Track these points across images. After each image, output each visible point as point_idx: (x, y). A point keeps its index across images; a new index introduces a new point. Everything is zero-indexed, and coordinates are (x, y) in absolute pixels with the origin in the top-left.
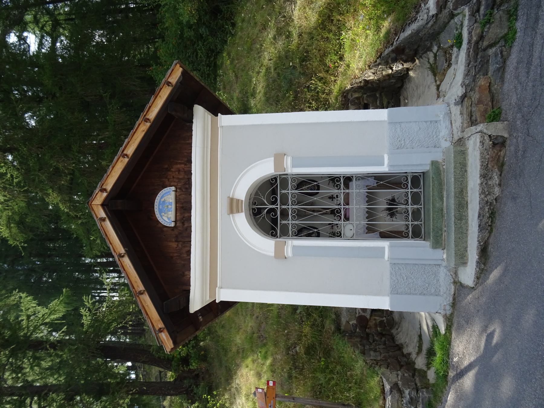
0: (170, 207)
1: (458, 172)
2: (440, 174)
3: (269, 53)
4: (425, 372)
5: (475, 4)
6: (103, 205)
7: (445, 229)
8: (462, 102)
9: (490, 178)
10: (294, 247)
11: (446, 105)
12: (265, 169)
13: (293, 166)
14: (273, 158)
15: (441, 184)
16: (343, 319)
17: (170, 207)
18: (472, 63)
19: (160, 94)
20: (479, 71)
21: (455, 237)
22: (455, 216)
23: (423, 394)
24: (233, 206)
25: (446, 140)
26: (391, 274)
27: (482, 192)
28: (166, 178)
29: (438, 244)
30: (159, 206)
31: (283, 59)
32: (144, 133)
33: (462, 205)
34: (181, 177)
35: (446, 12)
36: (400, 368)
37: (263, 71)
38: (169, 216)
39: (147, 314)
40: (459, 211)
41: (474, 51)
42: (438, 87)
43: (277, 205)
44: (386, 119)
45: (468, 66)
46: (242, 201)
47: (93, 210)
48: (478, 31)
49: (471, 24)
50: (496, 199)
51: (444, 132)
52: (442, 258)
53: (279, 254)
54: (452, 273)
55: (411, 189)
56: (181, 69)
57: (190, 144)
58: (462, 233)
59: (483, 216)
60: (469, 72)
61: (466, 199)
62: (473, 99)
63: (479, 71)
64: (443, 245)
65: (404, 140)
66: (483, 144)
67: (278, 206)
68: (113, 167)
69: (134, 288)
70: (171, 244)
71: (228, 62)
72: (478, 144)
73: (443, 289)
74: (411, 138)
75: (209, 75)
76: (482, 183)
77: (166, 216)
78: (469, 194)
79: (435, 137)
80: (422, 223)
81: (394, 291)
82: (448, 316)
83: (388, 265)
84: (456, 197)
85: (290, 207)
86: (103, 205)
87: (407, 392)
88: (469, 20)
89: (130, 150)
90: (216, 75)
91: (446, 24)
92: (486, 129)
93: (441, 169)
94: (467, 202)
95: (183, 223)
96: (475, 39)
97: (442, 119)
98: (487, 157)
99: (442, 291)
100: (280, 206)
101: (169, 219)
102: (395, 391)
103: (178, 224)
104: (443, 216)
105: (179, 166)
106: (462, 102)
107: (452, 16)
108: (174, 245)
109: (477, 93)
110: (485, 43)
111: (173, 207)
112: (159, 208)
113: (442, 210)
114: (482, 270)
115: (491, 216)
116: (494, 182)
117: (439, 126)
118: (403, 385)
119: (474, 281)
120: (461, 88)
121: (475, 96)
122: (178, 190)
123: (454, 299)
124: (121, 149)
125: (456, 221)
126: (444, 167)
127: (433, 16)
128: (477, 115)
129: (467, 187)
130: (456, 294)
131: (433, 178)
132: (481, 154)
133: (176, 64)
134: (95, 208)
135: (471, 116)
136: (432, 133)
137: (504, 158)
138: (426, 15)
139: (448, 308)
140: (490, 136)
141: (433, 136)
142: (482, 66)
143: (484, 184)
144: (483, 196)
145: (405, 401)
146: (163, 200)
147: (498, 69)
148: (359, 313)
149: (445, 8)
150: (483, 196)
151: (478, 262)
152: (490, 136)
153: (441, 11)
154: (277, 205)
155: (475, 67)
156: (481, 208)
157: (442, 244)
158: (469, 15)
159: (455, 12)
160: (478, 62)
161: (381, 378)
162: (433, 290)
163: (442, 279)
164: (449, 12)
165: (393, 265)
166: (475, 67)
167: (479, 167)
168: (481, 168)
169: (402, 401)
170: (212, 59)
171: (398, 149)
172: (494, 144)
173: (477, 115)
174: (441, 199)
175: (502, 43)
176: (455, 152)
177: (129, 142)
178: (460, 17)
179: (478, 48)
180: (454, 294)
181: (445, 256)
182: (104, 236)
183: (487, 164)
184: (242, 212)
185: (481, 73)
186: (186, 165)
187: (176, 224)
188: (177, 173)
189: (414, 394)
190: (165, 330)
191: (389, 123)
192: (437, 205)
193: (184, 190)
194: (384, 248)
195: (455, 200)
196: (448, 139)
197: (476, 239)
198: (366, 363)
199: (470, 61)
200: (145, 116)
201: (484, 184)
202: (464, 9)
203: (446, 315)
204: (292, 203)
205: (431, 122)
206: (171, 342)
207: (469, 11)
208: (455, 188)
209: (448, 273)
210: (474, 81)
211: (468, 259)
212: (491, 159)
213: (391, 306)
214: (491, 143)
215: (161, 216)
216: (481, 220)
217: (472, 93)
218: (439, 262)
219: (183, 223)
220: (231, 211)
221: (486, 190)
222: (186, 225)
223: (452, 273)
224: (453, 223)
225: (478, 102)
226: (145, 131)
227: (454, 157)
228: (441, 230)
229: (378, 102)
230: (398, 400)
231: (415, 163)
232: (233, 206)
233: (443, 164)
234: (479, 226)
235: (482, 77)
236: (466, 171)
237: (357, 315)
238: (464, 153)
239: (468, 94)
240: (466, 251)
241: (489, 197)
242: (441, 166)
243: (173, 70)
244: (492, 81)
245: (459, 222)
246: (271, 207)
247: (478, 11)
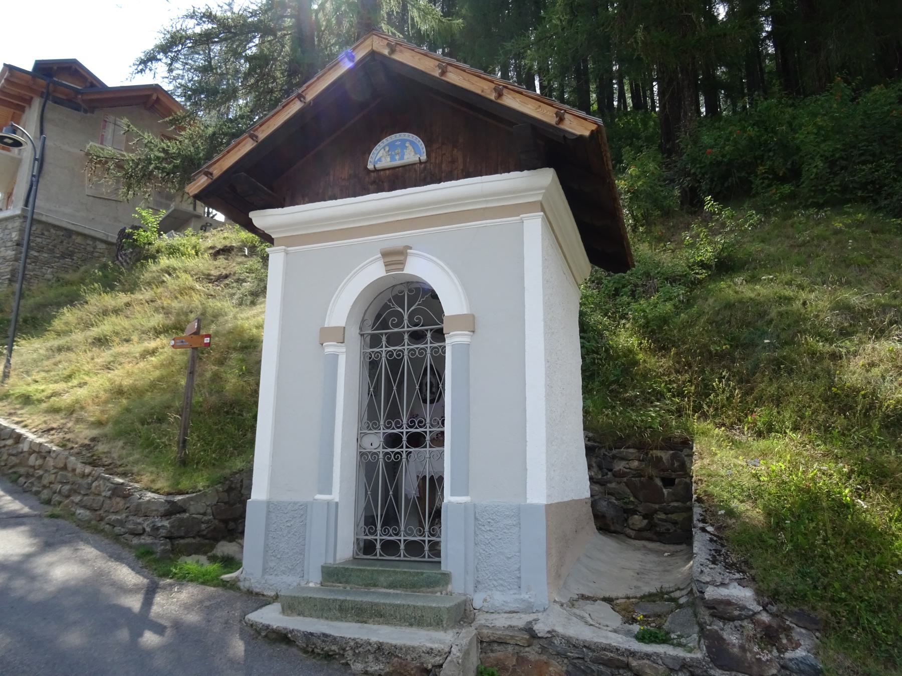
0: (397, 157)
1: (409, 612)
2: (428, 586)
3: (818, 301)
4: (205, 553)
5: (706, 671)
6: (373, 54)
7: (348, 588)
9: (377, 659)
10: (335, 357)
12: (453, 303)
14: (465, 312)
15: (413, 586)
17: (397, 157)
18: (590, 654)
20: (574, 665)
21: (315, 599)
23: (162, 545)
24: (394, 257)
25: (485, 600)
26: (295, 503)
27: (358, 644)
28: (443, 144)
30: (399, 140)
31: (795, 325)
32: (479, 92)
33: (362, 614)
34: (444, 166)
36: (221, 520)
37: (789, 292)
38: (383, 159)
41: (611, 660)
42: (608, 600)
43: (408, 327)
44: (528, 501)
45: (585, 646)
46: (402, 269)
47: (365, 40)
49: (667, 661)
50: (347, 664)
51: (499, 598)
55: (429, 541)
56: (587, 133)
57: (496, 172)
59: (324, 641)
60: (574, 646)
62: (527, 649)
63: (574, 665)
66: (428, 653)
67: (406, 329)
69: (261, 126)
71: (839, 225)
72: (429, 645)
73: (272, 579)
74: (493, 543)
75: (824, 191)
76: (370, 644)
77: (381, 157)
78: (376, 627)
79: (495, 583)
80: (378, 557)
81: (271, 507)
84: (373, 605)
85: (406, 347)
87: (166, 523)
88: (675, 658)
90: (820, 207)
93: (437, 589)
94: (366, 623)
95: (374, 182)
96: (634, 663)
97: (522, 597)
98: (409, 657)
99: (270, 577)
100: (408, 332)
101: (380, 160)
102: (168, 507)
105: (460, 160)
109: (537, 657)
111: (398, 162)
112: (396, 141)
113: (375, 585)
117: (512, 592)
118: (182, 520)
120: (547, 629)
121: (532, 654)
123: (257, 594)
124: (453, 61)
126: (439, 594)
128: (499, 653)
130: (261, 598)
131: (422, 574)
132: (413, 647)
133: (595, 123)
134: (368, 42)
135: (500, 643)
136: (501, 579)
138: (708, 579)
139: (247, 584)
140: (441, 666)
142: (584, 671)
143: (369, 647)
144: (352, 644)
149: (713, 615)
150: (352, 644)
153: (709, 608)
154: (408, 327)
155: (583, 659)
156: (335, 638)
158: (684, 659)
161: (200, 491)
162: (272, 564)
163: (285, 578)
166: (583, 659)
167: (394, 642)
170: (860, 193)
171: (476, 519)
173: (499, 653)
174: (391, 586)
176: (439, 609)
177: (464, 71)
179: (618, 668)
180: (263, 595)
181: (311, 585)
182: (328, 66)
183: (397, 656)
184: (387, 271)
185: (570, 668)
186: (462, 170)
187: (373, 171)
188: (450, 159)
189: (163, 532)
190: (210, 181)
192: (382, 579)
193: (423, 175)
194: (330, 493)
195: (368, 603)
196: (485, 604)
197: (296, 628)
198: (236, 473)
199: (593, 651)
200: (506, 87)
201: (369, 647)
203: (239, 581)
206: (196, 192)
207: (692, 659)
212: (404, 663)
213: (253, 501)
214: (430, 667)
215: (384, 147)
216: (319, 637)
217: (537, 648)
218: (306, 577)
219: (374, 182)
220: (385, 254)
221: (360, 649)
222: (371, 187)
224: (336, 597)
225: (522, 658)
226: (483, 94)
227: (430, 608)
228: (347, 582)
229: (676, 504)
232: (394, 257)
233: (444, 592)
234: (312, 634)
235: (564, 669)
236: (411, 625)
238: (438, 624)
239: (535, 641)
240: (299, 615)
241: (350, 653)
243: (586, 119)
246: (406, 317)
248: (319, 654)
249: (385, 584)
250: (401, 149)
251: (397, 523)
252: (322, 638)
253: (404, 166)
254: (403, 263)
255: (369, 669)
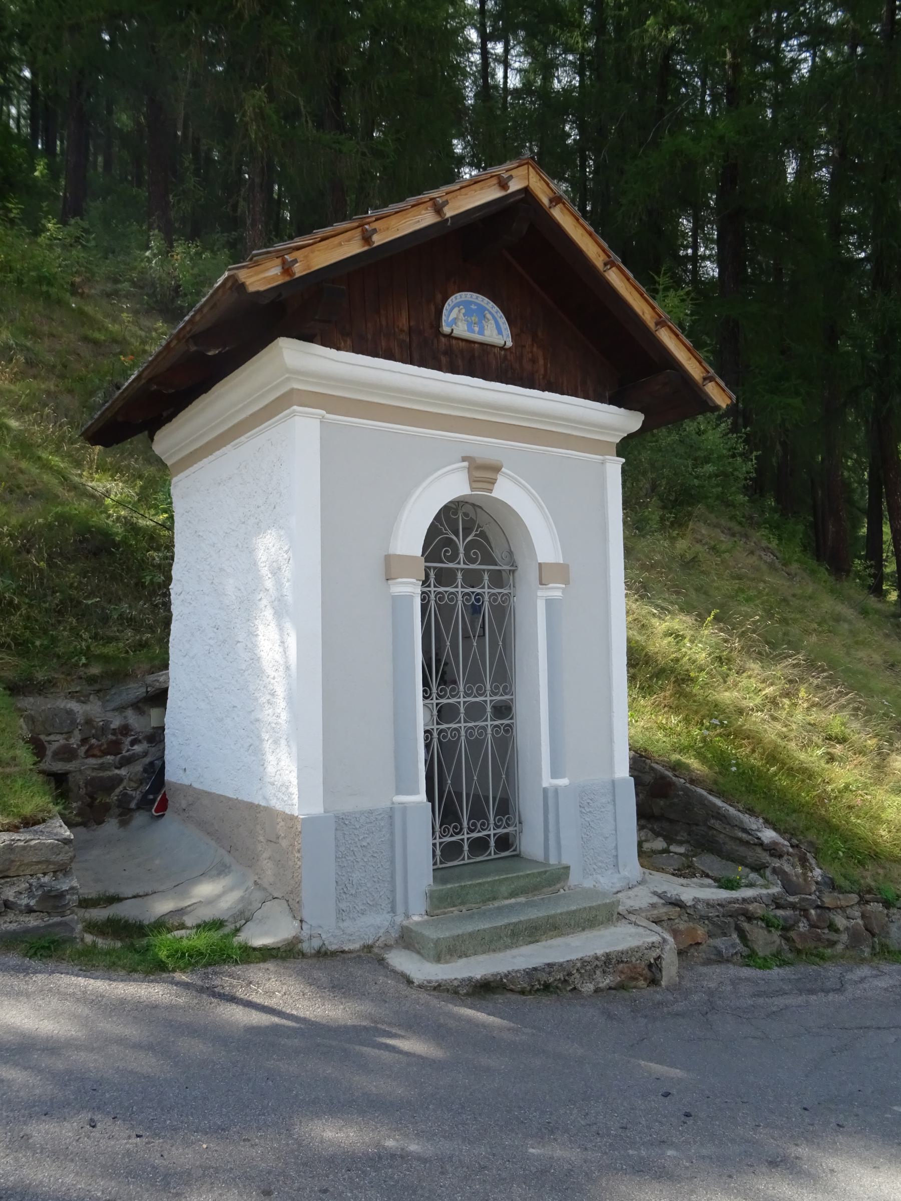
1: (584, 916)
8: (671, 903)
11: (640, 879)
13: (549, 603)
16: (31, 699)
19: (693, 359)
22: (520, 922)
26: (371, 812)
29: (439, 902)
30: (476, 304)
32: (641, 314)
33: (533, 932)
35: (765, 857)
39: (323, 239)
40: (526, 929)
45: (719, 905)
46: (491, 491)
48: (759, 911)
50: (575, 988)
52: (411, 913)
53: (392, 567)
54: (383, 939)
58: (491, 942)
61: (544, 937)
63: (713, 923)
64: (439, 911)
65: (590, 812)
67: (462, 566)
68: (590, 234)
70: (405, 315)
78: (550, 942)
82: (300, 946)
83: (385, 804)
86: (526, 190)
89: (614, 277)
91: (742, 862)
92: (670, 949)
93: (558, 886)
94: (537, 941)
100: (462, 569)
103: (443, 339)
104: (484, 902)
105: (541, 362)
106: (671, 903)
107: (759, 868)
108: (403, 322)
110: (746, 926)
112: (471, 303)
113: (494, 899)
114: (456, 993)
115: (548, 985)
116: (600, 979)
117: (609, 872)
119: (429, 982)
120: (691, 897)
122: (503, 353)
123: (334, 954)
125: (511, 927)
126: (562, 891)
127: (759, 838)
129: (561, 935)
133: (731, 398)
137: (635, 987)
139: (316, 943)
141: (595, 864)
143: (597, 963)
144: (579, 965)
145: (46, 879)
146: (488, 316)
147: (719, 953)
148: (49, 742)
149: (772, 855)
151: (470, 979)
152: (659, 957)
153: (765, 850)
156: (561, 965)
157: (439, 908)
159: (768, 872)
160: (722, 919)
164: (768, 862)
165: (390, 814)
168: (618, 952)
169: (45, 874)
172: (650, 966)
174: (512, 895)
175: (746, 951)
178: (761, 881)
180: (343, 952)
181: (416, 918)
184: (472, 489)
185: (710, 927)
187: (445, 336)
190: (287, 279)
191: (613, 782)
197: (510, 969)
201: (597, 963)
202: (775, 884)
203: (301, 941)
204: (439, 593)
205: (617, 856)
208: (561, 914)
209: (382, 931)
210: (702, 917)
211: (447, 962)
215: (458, 305)
218: (400, 909)
222: (444, 359)
223: (383, 939)
228: (463, 903)
230: (48, 862)
231: (562, 836)
232: (484, 472)
233: (566, 888)
234: (535, 969)
235: (706, 929)
237: (42, 737)
240: (460, 957)
241: (577, 975)
242: (562, 884)
243: (724, 391)
244: (701, 947)
245: (509, 932)
246: (461, 550)
247: (779, 906)
248: (538, 990)
249: (506, 894)
250: (474, 317)
251: (459, 820)
252: (547, 970)
253: (482, 344)
254: (493, 482)
255: (601, 985)
